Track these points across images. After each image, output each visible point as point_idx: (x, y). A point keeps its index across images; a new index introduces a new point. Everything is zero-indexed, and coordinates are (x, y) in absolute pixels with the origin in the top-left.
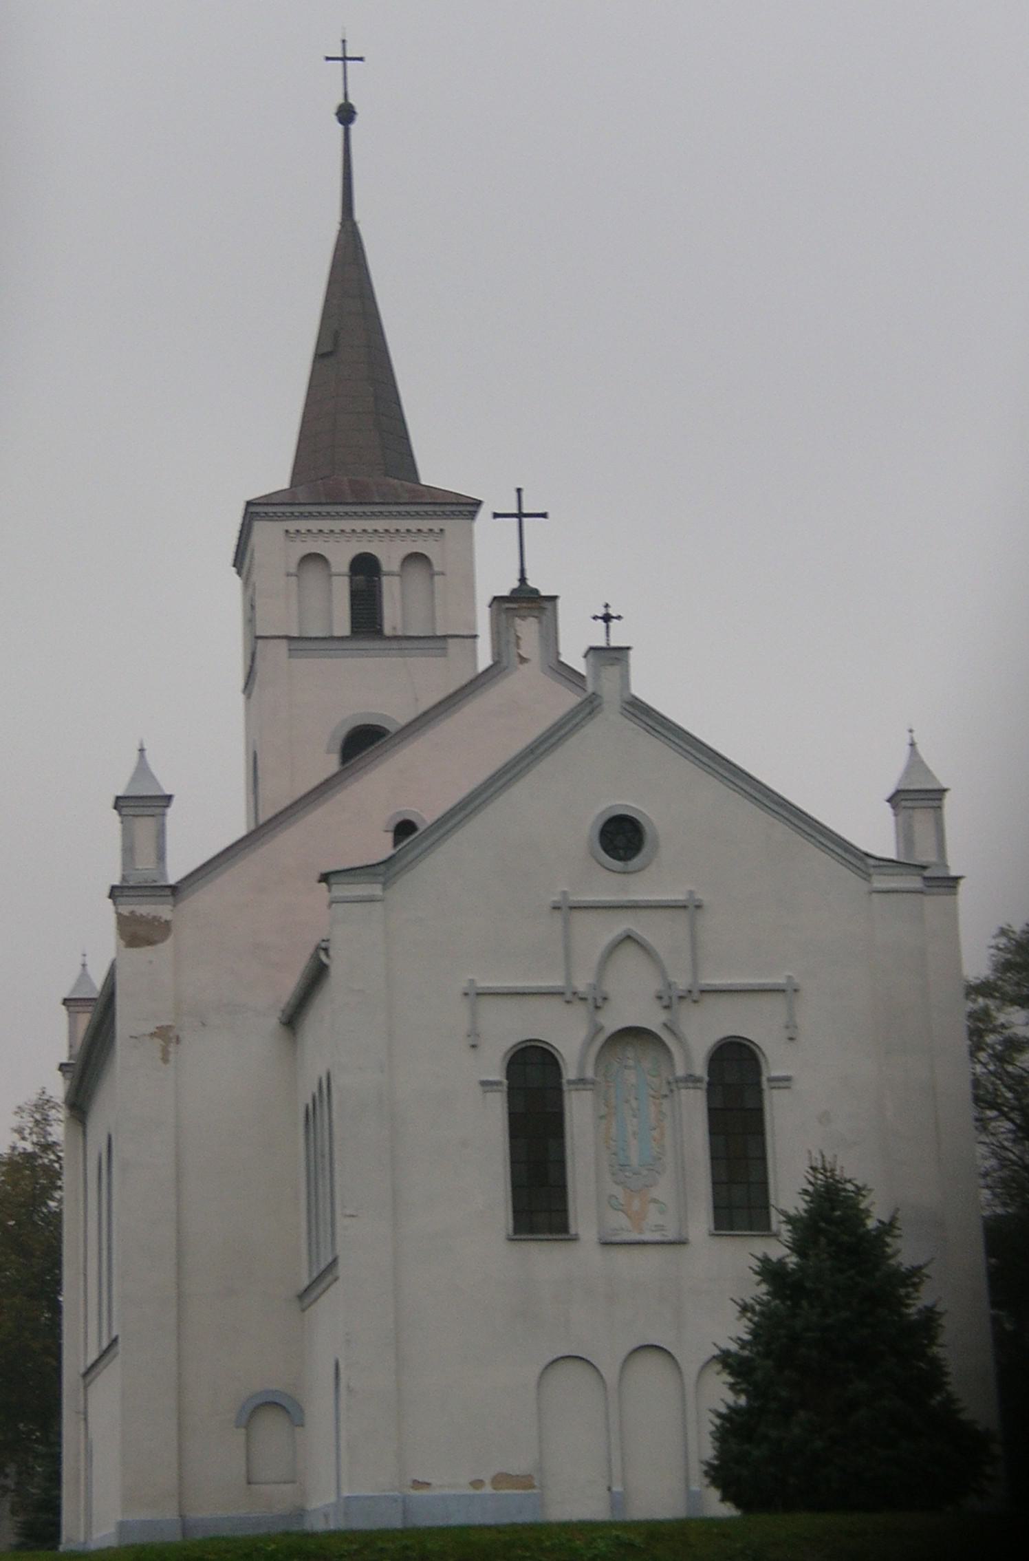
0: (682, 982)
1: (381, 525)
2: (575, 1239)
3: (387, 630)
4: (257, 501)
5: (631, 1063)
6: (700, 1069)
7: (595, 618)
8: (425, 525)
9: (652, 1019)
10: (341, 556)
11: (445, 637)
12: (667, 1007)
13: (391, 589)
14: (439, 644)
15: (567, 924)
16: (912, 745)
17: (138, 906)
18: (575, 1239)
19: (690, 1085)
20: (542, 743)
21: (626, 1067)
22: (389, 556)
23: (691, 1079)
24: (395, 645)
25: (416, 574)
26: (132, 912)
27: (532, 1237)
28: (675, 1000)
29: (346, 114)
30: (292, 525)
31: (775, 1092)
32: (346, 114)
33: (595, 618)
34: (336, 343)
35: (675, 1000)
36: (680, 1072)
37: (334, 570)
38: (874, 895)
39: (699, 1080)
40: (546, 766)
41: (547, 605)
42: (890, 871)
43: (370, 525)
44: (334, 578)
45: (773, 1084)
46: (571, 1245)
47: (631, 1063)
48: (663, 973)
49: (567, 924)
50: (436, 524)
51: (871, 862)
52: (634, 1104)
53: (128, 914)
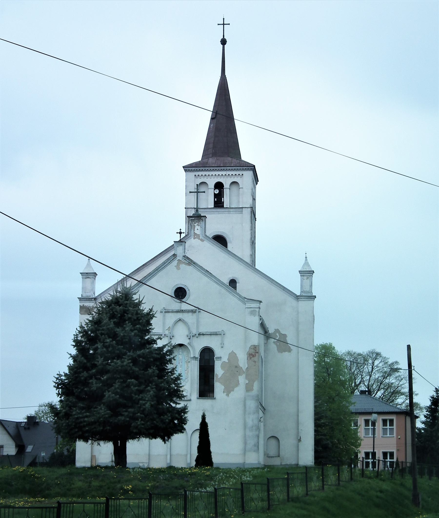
0: (194, 331)
1: (224, 173)
2: (215, 399)
3: (225, 206)
4: (186, 166)
5: (181, 353)
6: (198, 355)
7: (177, 233)
8: (237, 173)
9: (185, 342)
10: (212, 183)
11: (242, 208)
12: (190, 339)
13: (226, 192)
14: (240, 210)
15: (164, 316)
16: (306, 257)
17: (85, 303)
18: (215, 399)
19: (194, 359)
20: (160, 268)
21: (179, 354)
22: (226, 183)
23: (195, 358)
24: (227, 210)
25: (234, 187)
26: (83, 305)
27: (202, 398)
28: (191, 337)
29: (224, 42)
30: (197, 173)
31: (217, 361)
32: (224, 42)
33: (177, 233)
34: (216, 116)
35: (191, 337)
36: (192, 356)
37: (209, 187)
38: (246, 309)
39: (197, 358)
40: (161, 274)
41: (204, 218)
42: (250, 302)
43: (220, 173)
44: (209, 189)
45: (217, 359)
46: (213, 400)
47: (181, 353)
48: (189, 329)
49: (164, 316)
50: (241, 173)
51: (246, 300)
52: (181, 364)
53: (82, 306)
